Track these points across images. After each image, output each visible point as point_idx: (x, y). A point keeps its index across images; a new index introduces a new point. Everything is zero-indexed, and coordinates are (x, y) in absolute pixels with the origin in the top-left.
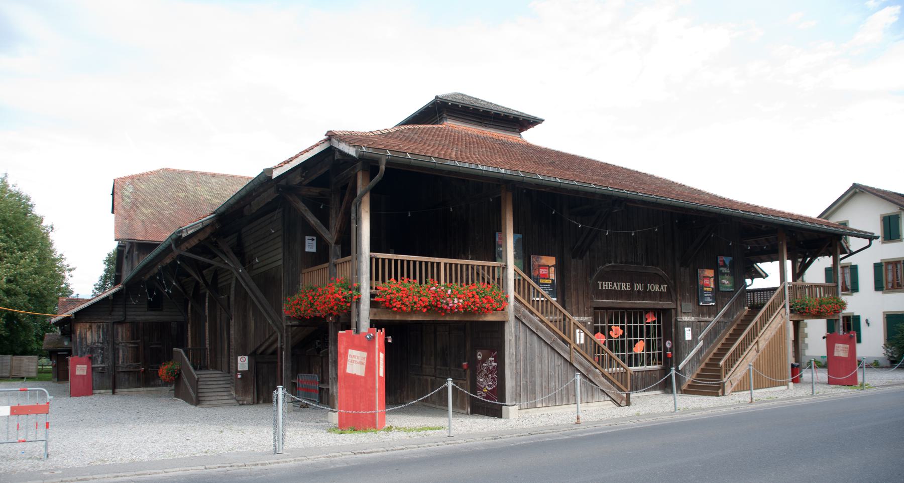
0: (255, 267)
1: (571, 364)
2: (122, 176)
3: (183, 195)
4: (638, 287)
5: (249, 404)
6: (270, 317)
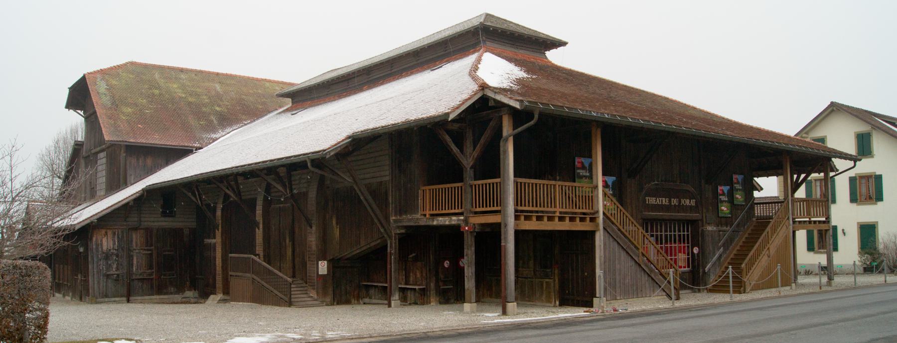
3: (157, 92)
4: (675, 202)
5: (327, 305)
6: (383, 227)
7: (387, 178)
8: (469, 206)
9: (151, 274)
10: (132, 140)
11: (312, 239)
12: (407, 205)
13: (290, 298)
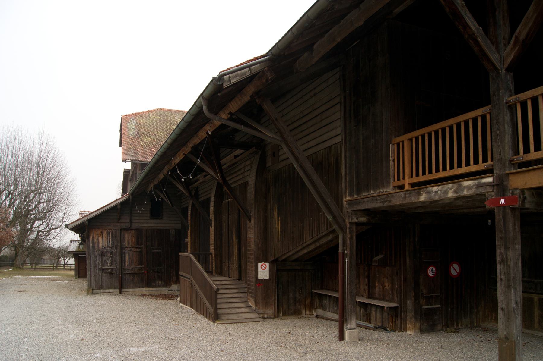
0: (282, 158)
2: (128, 113)
6: (331, 212)
7: (338, 139)
8: (508, 152)
9: (140, 270)
10: (143, 160)
11: (252, 236)
12: (371, 173)
13: (216, 309)
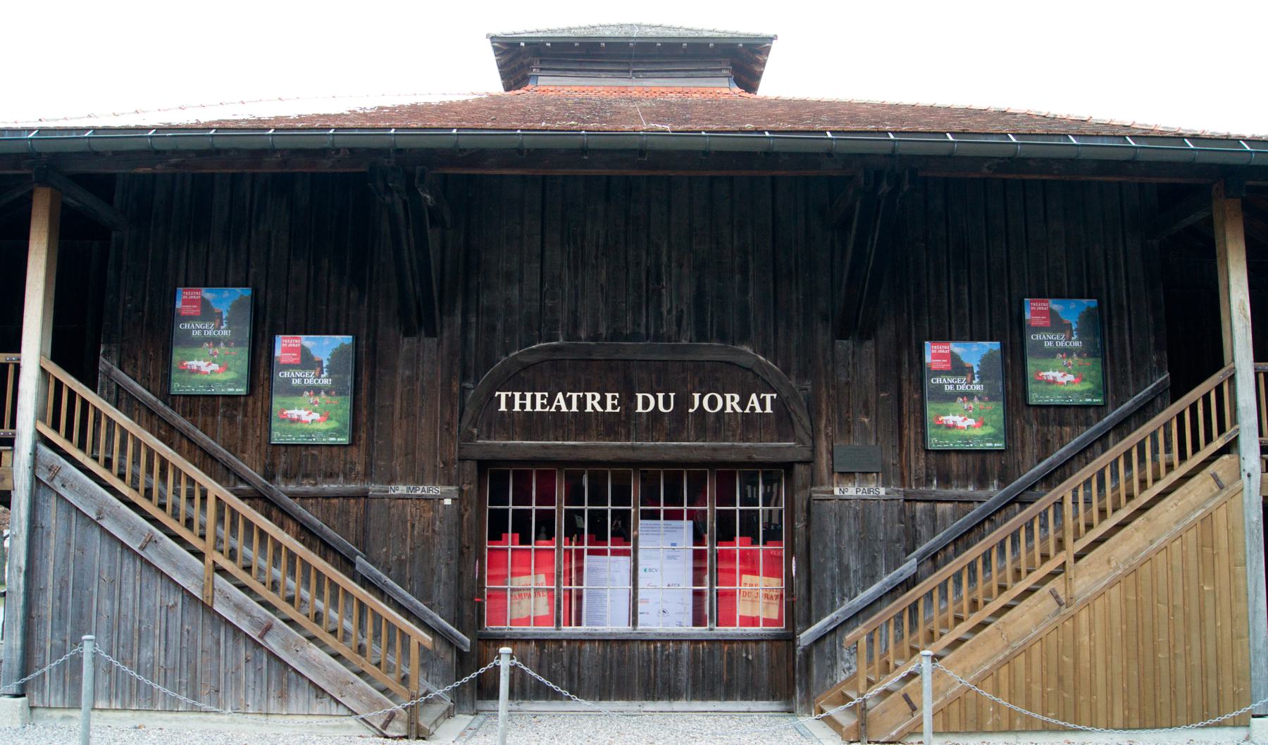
1: (208, 609)
4: (650, 402)
